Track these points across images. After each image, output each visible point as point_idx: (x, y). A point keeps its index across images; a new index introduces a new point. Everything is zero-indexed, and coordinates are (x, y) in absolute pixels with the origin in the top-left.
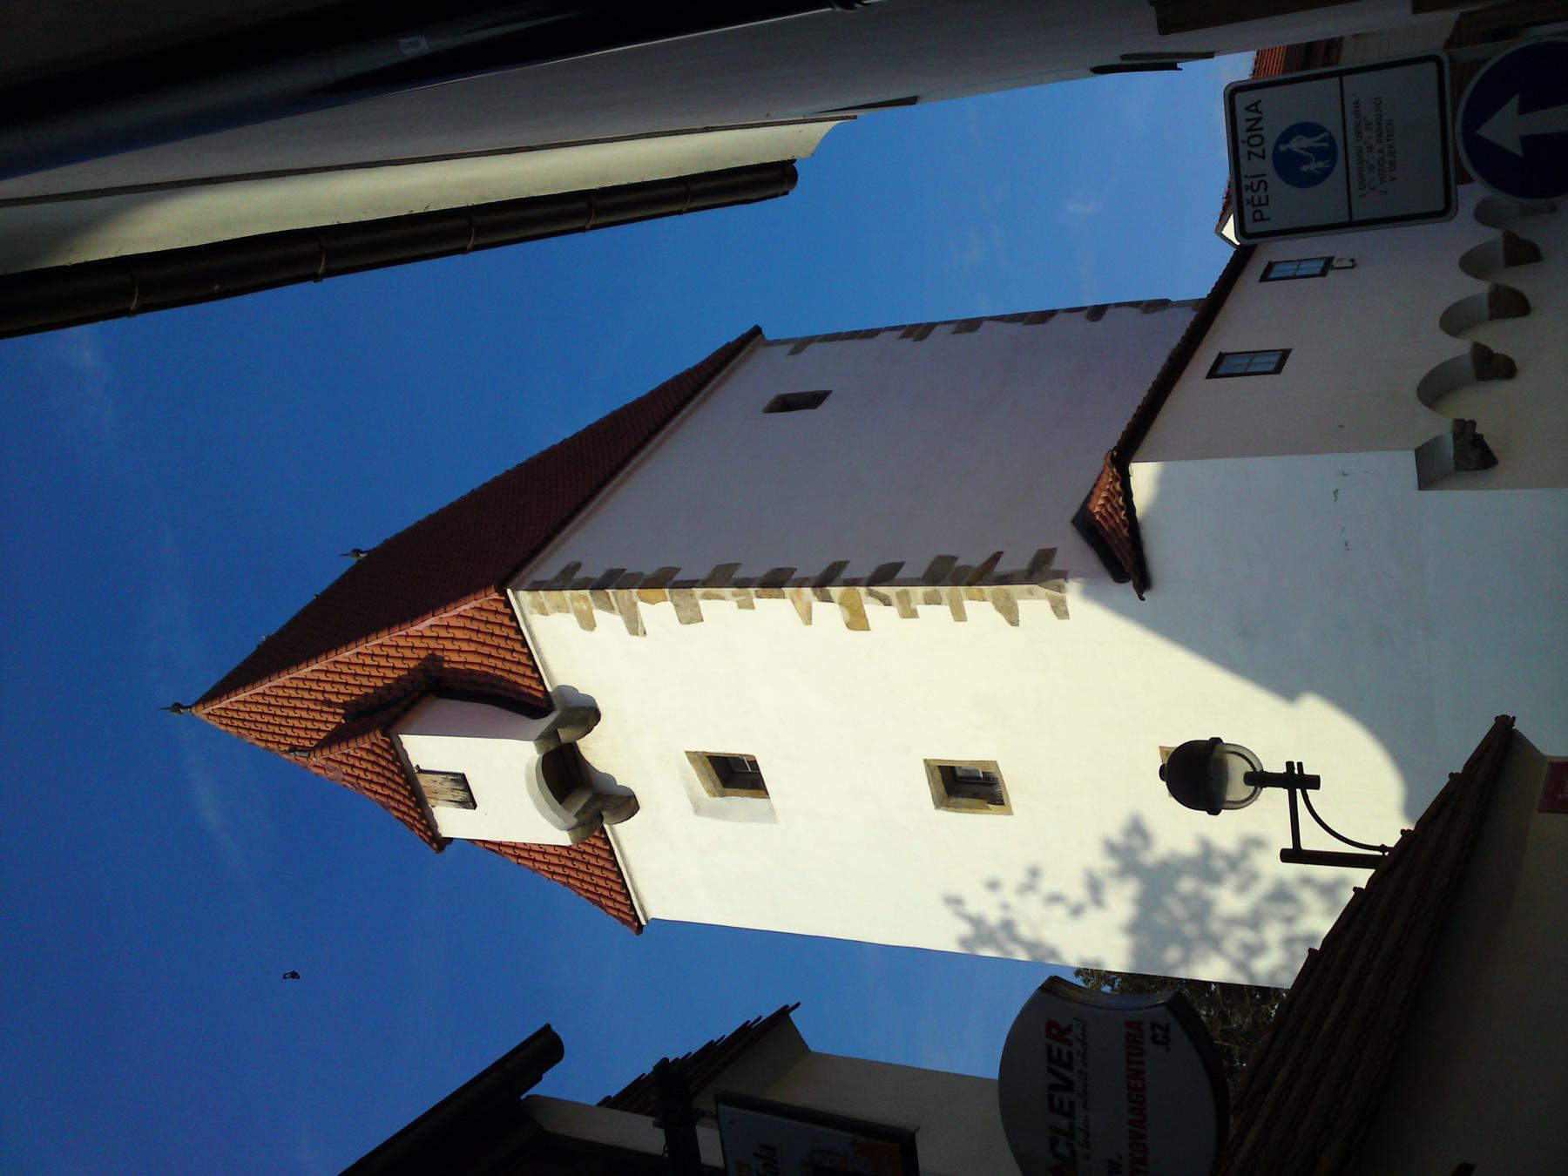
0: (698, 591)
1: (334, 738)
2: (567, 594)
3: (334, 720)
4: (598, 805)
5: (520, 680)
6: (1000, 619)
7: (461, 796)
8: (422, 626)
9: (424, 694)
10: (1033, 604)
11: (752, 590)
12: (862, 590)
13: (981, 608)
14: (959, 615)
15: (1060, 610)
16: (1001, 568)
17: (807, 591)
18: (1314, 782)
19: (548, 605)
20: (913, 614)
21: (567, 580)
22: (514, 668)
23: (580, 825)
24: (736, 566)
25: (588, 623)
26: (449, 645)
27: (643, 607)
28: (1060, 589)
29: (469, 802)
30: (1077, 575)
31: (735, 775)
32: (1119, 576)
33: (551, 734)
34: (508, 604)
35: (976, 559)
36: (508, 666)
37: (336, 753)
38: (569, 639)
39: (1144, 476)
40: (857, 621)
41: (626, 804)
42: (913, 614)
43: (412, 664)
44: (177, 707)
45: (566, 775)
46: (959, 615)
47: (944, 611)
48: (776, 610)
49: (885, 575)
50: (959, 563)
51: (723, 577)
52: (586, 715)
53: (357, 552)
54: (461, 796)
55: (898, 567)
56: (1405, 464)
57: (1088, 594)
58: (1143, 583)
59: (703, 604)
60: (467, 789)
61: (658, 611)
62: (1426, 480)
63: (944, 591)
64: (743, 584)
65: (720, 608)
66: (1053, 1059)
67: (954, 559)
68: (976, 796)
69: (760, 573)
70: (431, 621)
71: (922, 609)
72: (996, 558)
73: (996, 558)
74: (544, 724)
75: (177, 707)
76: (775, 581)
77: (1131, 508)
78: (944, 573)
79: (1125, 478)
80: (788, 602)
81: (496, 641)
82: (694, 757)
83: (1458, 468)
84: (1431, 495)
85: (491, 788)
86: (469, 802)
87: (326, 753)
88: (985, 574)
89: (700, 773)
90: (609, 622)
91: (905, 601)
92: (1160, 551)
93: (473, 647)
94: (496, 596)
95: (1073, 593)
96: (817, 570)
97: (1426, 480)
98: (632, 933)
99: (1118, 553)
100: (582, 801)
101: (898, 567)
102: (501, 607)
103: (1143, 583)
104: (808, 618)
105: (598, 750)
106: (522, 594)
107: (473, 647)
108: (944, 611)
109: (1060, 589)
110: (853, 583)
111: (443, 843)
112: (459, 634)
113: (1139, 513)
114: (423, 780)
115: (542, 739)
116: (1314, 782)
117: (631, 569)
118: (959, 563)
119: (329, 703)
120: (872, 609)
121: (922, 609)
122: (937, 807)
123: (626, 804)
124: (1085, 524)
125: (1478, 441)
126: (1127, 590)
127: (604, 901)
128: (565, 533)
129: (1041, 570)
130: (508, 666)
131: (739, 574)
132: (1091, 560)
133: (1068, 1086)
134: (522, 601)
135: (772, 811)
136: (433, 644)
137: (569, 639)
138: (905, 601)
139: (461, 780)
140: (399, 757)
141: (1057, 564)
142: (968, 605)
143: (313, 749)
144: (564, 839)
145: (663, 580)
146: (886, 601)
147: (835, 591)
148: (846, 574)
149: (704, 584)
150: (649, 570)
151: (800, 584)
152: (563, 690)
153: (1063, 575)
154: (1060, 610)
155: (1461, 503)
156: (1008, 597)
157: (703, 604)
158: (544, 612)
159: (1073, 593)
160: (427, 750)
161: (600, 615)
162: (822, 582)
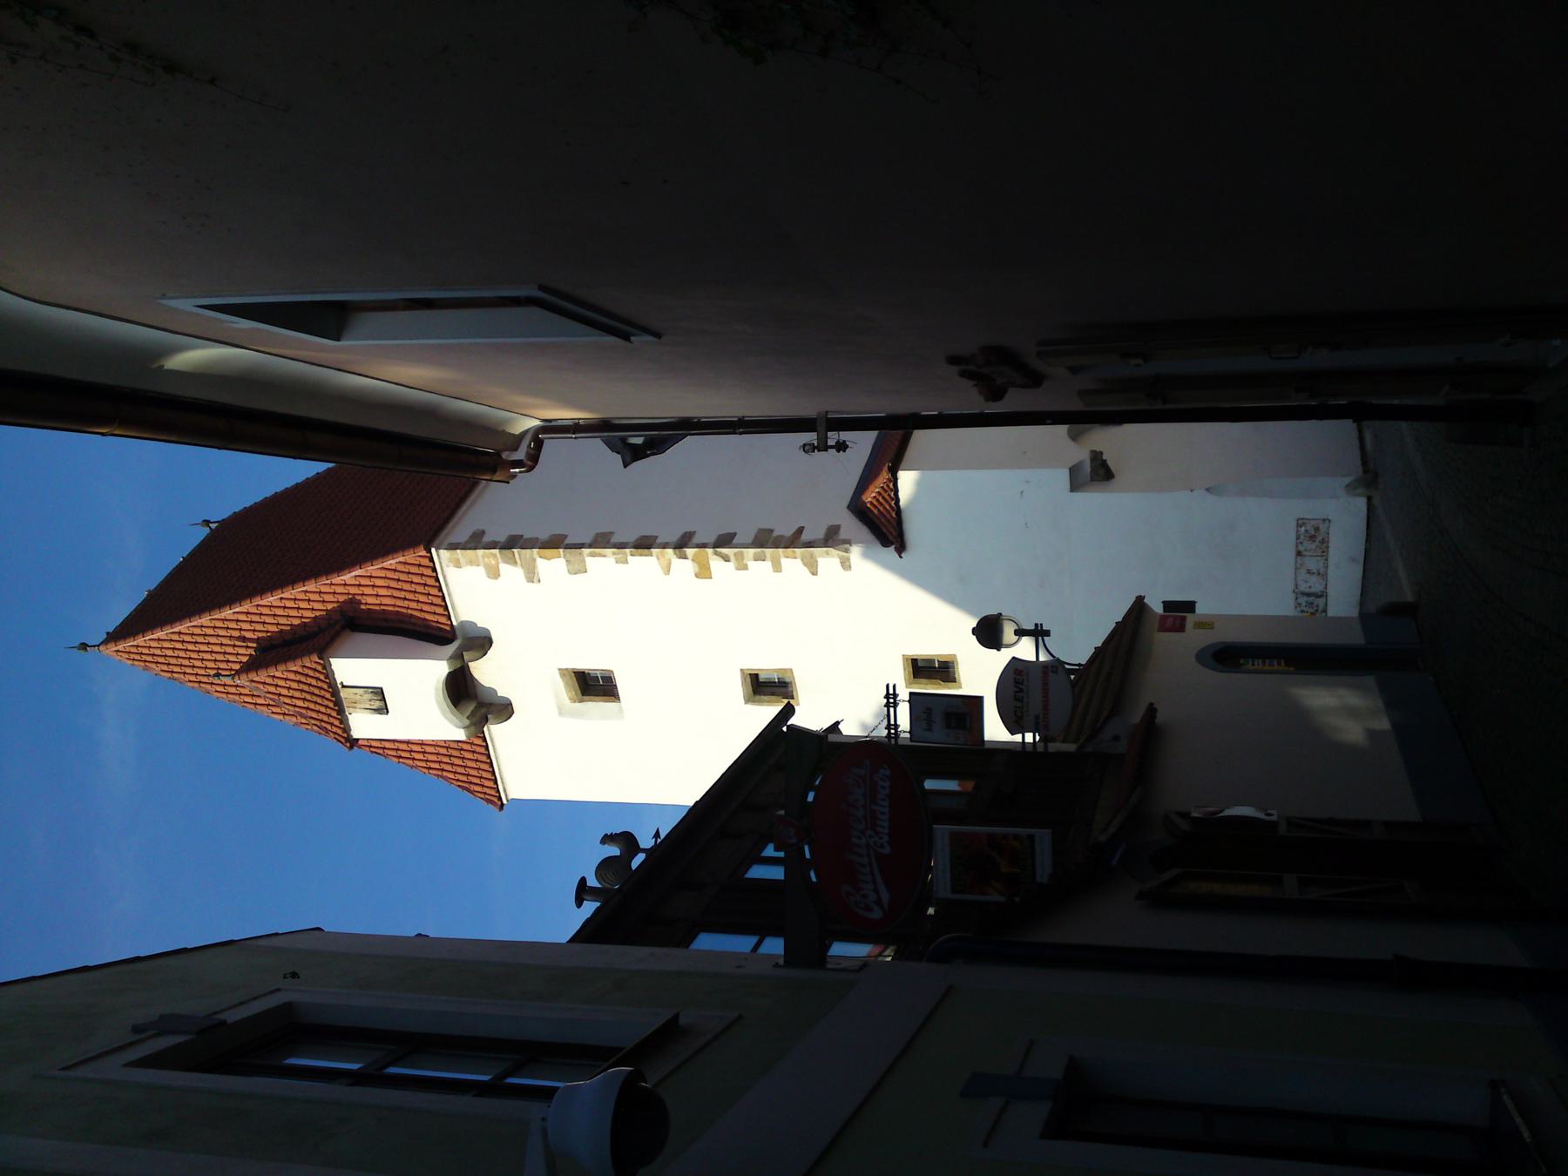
0: (586, 551)
1: (251, 666)
2: (480, 552)
3: (245, 653)
4: (483, 711)
5: (428, 617)
6: (806, 571)
7: (378, 704)
8: (347, 577)
9: (343, 628)
10: (828, 560)
11: (628, 551)
12: (710, 551)
13: (792, 563)
14: (777, 568)
15: (846, 565)
16: (805, 537)
17: (670, 551)
18: (1047, 633)
19: (462, 560)
20: (745, 568)
21: (476, 541)
22: (426, 608)
23: (472, 724)
24: (612, 533)
25: (494, 574)
26: (368, 591)
27: (540, 562)
28: (847, 551)
29: (384, 710)
30: (857, 542)
31: (593, 686)
32: (885, 542)
33: (458, 656)
34: (431, 560)
35: (788, 532)
36: (420, 606)
37: (262, 676)
38: (471, 585)
39: (907, 481)
40: (704, 572)
41: (504, 710)
42: (745, 568)
43: (330, 607)
44: (84, 646)
45: (460, 689)
46: (777, 568)
47: (767, 565)
48: (645, 565)
49: (725, 541)
50: (775, 534)
51: (602, 541)
52: (481, 642)
53: (207, 522)
54: (378, 704)
55: (733, 535)
56: (1063, 476)
57: (865, 555)
58: (901, 548)
59: (589, 560)
60: (384, 699)
61: (552, 566)
62: (1074, 487)
63: (769, 551)
64: (621, 546)
65: (602, 564)
66: (1017, 682)
67: (772, 531)
68: (773, 694)
69: (632, 537)
70: (358, 572)
71: (751, 564)
72: (800, 530)
73: (800, 530)
74: (451, 649)
75: (84, 646)
76: (644, 544)
77: (897, 500)
78: (765, 540)
79: (895, 480)
80: (653, 559)
81: (414, 587)
82: (563, 672)
83: (1092, 479)
84: (1077, 496)
85: (401, 696)
86: (384, 710)
87: (253, 676)
88: (794, 541)
89: (566, 684)
90: (511, 573)
91: (740, 558)
92: (914, 529)
93: (389, 592)
94: (424, 553)
95: (855, 552)
96: (675, 537)
97: (1074, 487)
98: (496, 810)
99: (886, 529)
100: (471, 707)
101: (733, 535)
102: (426, 562)
103: (901, 548)
104: (667, 570)
105: (484, 671)
106: (442, 552)
107: (389, 592)
108: (767, 565)
109: (847, 551)
110: (703, 546)
111: (353, 743)
112: (379, 582)
113: (902, 503)
114: (344, 694)
115: (452, 658)
116: (1047, 633)
117: (528, 534)
118: (775, 534)
119: (244, 639)
120: (716, 564)
121: (751, 564)
122: (747, 701)
123: (504, 710)
124: (858, 509)
125: (1104, 464)
126: (890, 552)
127: (473, 787)
128: (464, 508)
129: (832, 538)
130: (420, 606)
131: (614, 540)
132: (864, 532)
133: (1021, 691)
134: (442, 557)
135: (621, 710)
136: (353, 590)
137: (471, 585)
138: (740, 558)
139: (379, 693)
140: (329, 675)
141: (843, 535)
142: (784, 561)
143: (238, 672)
144: (460, 735)
145: (554, 543)
146: (727, 559)
147: (690, 552)
148: (696, 540)
149: (590, 546)
150: (544, 536)
151: (664, 546)
152: (462, 623)
153: (849, 542)
154: (846, 565)
155: (1095, 500)
156: (812, 556)
157: (589, 560)
158: (458, 565)
159: (855, 552)
160: (349, 670)
161: (505, 568)
162: (681, 544)
